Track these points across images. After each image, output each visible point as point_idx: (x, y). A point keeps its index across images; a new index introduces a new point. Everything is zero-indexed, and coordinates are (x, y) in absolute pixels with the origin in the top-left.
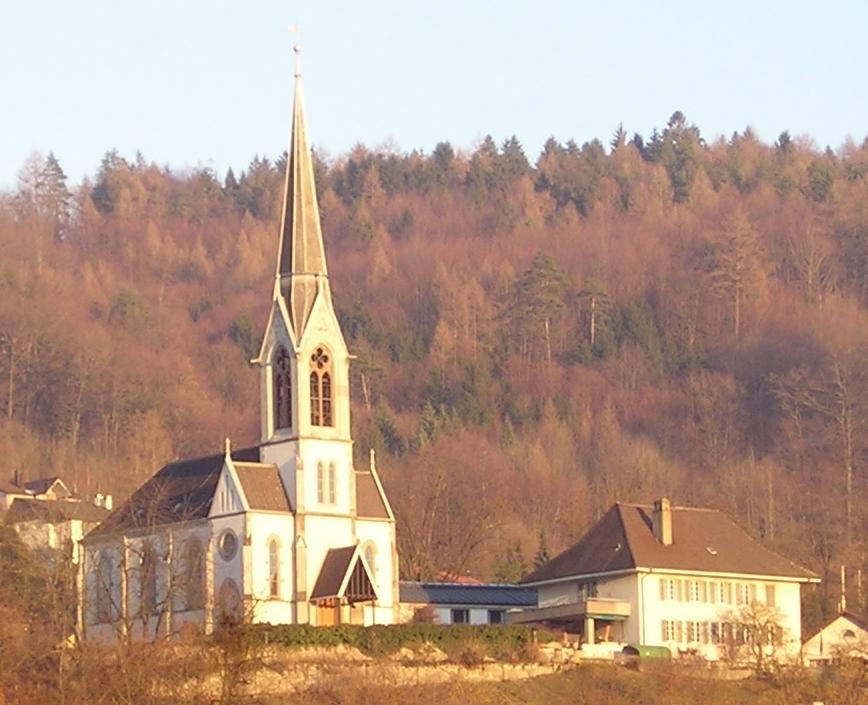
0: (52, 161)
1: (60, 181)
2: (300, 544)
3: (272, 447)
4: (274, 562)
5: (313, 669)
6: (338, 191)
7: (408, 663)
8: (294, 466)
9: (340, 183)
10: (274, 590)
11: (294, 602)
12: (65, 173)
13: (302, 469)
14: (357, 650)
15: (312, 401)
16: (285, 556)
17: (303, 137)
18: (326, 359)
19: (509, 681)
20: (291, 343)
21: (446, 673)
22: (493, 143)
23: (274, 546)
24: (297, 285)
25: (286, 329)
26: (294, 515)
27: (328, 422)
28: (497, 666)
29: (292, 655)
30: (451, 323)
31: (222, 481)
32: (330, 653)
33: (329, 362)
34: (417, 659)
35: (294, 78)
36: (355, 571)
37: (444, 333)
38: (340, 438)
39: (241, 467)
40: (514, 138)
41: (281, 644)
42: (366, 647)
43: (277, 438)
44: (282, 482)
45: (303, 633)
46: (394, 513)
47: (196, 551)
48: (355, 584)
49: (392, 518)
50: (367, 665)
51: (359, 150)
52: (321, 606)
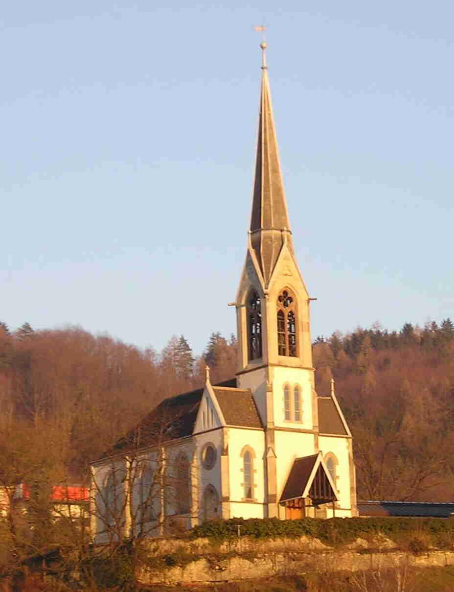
0: (183, 341)
1: (187, 352)
2: (270, 454)
3: (246, 374)
4: (248, 470)
5: (280, 557)
6: (347, 351)
7: (362, 551)
8: (266, 388)
9: (348, 346)
10: (249, 494)
11: (266, 504)
12: (190, 348)
13: (271, 391)
14: (318, 541)
15: (279, 334)
16: (258, 464)
17: (269, 118)
18: (291, 300)
19: (450, 565)
20: (261, 286)
21: (397, 558)
22: (436, 326)
23: (248, 456)
24: (265, 238)
25: (256, 275)
26: (265, 431)
27: (293, 353)
28: (440, 554)
29: (263, 545)
30: (413, 415)
31: (204, 400)
32: (295, 543)
33: (293, 303)
34: (372, 547)
35: (261, 70)
36: (317, 474)
37: (408, 419)
38: (304, 366)
39: (216, 390)
40: (448, 320)
41: (253, 535)
42: (326, 538)
43: (251, 367)
44: (255, 404)
45: (271, 526)
46: (351, 430)
47: (183, 467)
48: (317, 489)
49: (350, 435)
50: (327, 553)
51: (360, 330)
52: (289, 507)
